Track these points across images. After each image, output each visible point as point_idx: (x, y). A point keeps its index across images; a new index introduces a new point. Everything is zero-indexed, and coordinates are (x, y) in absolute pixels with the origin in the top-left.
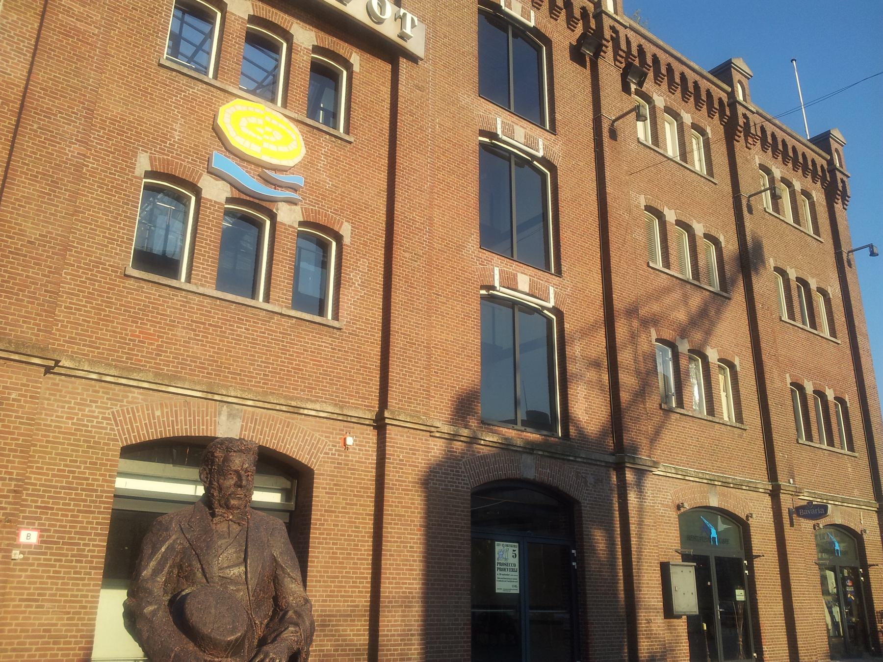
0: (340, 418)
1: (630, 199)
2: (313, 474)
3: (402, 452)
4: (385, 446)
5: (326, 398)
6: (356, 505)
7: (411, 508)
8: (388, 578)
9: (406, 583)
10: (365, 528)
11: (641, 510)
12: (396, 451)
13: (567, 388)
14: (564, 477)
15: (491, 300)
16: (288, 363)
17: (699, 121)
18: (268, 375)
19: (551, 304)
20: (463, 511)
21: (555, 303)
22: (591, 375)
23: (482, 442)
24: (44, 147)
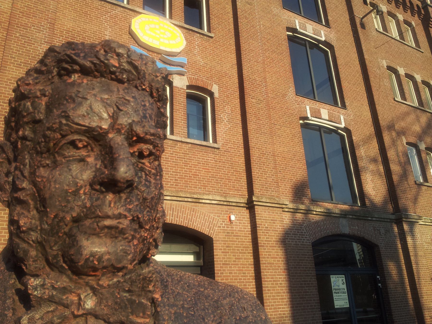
0: (225, 203)
1: (378, 63)
2: (213, 241)
3: (267, 222)
4: (255, 219)
5: (215, 192)
6: (242, 259)
7: (277, 258)
8: (269, 306)
9: (280, 308)
10: (249, 273)
11: (415, 247)
12: (263, 222)
13: (360, 175)
14: (367, 231)
15: (306, 127)
16: (189, 171)
17: (407, 18)
18: (177, 180)
19: (343, 126)
20: (308, 258)
21: (345, 125)
22: (372, 167)
23: (314, 213)
24: (24, 47)
